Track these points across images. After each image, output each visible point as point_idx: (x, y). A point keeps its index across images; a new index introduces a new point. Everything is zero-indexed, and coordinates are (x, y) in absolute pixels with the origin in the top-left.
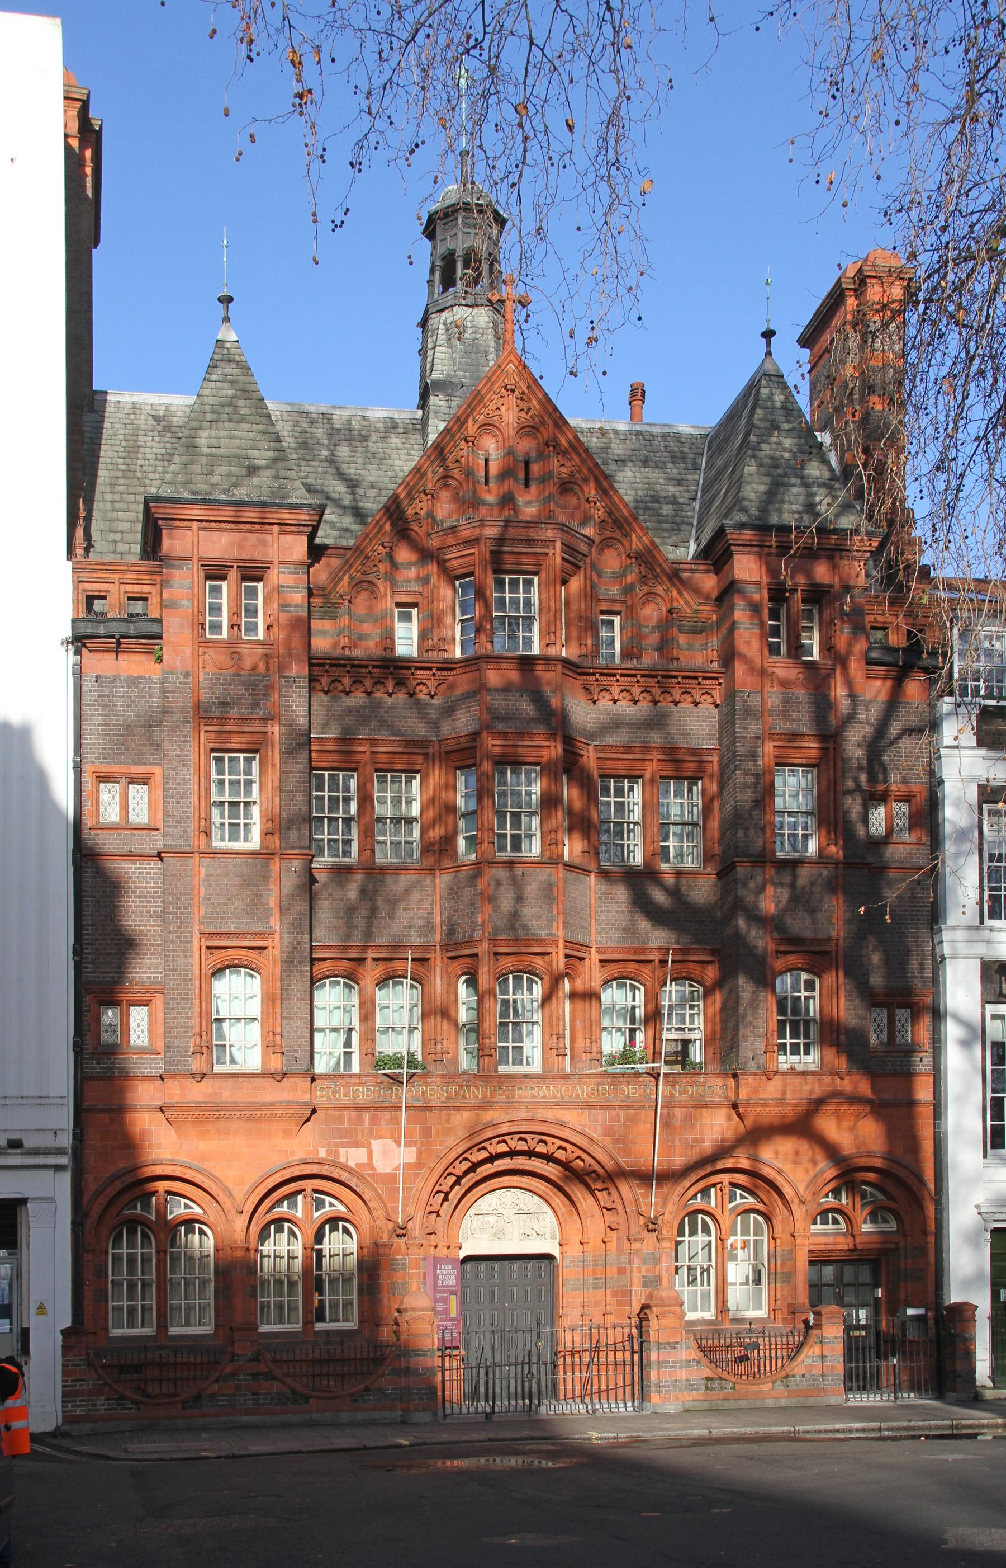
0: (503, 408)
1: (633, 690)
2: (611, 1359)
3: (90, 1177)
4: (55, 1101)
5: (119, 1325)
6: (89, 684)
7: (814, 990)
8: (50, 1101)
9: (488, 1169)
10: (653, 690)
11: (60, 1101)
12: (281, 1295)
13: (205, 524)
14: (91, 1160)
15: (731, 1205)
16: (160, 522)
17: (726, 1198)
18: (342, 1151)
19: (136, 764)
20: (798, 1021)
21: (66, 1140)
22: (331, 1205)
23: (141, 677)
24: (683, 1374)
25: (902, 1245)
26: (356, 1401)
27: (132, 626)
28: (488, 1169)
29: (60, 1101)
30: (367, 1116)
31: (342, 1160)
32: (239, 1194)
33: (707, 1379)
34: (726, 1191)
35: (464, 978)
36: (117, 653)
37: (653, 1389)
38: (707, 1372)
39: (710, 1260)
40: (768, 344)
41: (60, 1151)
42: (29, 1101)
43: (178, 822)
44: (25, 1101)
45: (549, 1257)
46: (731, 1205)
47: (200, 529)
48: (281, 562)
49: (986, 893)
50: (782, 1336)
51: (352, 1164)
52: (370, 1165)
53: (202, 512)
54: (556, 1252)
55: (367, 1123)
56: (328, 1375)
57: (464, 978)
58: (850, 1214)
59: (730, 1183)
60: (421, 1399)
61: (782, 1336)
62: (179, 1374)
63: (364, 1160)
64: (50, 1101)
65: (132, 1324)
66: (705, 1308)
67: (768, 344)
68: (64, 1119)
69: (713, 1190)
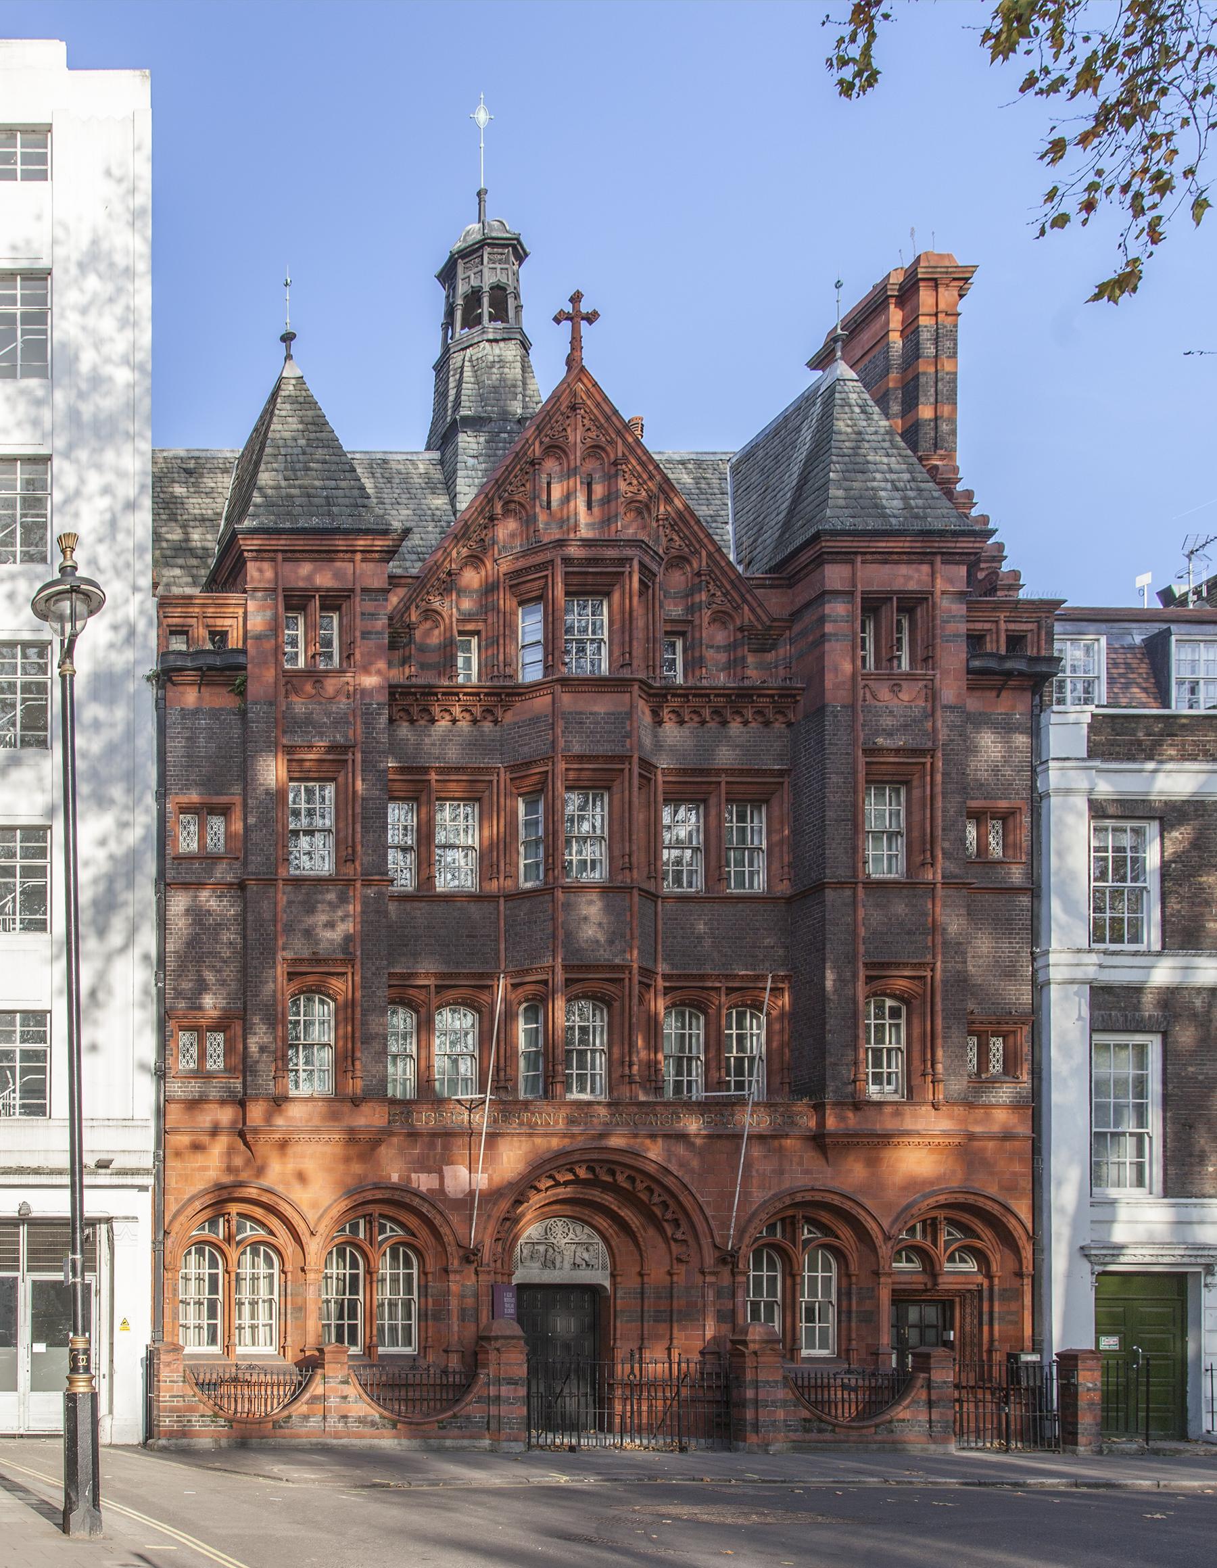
0: (569, 430)
1: (411, 709)
2: (839, 1396)
3: (170, 1198)
4: (140, 1123)
5: (811, 1346)
6: (173, 717)
7: (899, 1017)
8: (135, 1123)
9: (609, 1200)
10: (473, 709)
11: (144, 1123)
12: (813, 1321)
13: (289, 555)
14: (172, 1182)
15: (380, 1238)
16: (246, 554)
17: (376, 1230)
18: (413, 1176)
19: (217, 794)
20: (881, 1050)
21: (148, 1162)
22: (392, 1230)
23: (222, 709)
24: (781, 1414)
25: (985, 1287)
26: (444, 1427)
27: (218, 659)
28: (609, 1200)
29: (144, 1123)
30: (439, 1141)
31: (415, 1185)
32: (312, 1217)
33: (805, 1420)
34: (234, 1223)
35: (525, 1005)
36: (200, 685)
37: (749, 1428)
38: (805, 1414)
39: (271, 1293)
40: (288, 348)
41: (146, 1172)
42: (115, 1123)
43: (262, 850)
44: (111, 1123)
45: (593, 1290)
46: (380, 1238)
47: (285, 560)
48: (364, 590)
49: (48, 917)
50: (272, 1374)
51: (423, 1188)
52: (442, 1190)
53: (288, 542)
54: (607, 1284)
55: (439, 1150)
56: (399, 1400)
57: (525, 1005)
58: (367, 1249)
59: (238, 1214)
60: (511, 1428)
61: (272, 1374)
62: (411, 1394)
63: (435, 1185)
64: (135, 1123)
65: (394, 1343)
66: (408, 1343)
67: (288, 348)
68: (146, 1140)
69: (221, 1220)
